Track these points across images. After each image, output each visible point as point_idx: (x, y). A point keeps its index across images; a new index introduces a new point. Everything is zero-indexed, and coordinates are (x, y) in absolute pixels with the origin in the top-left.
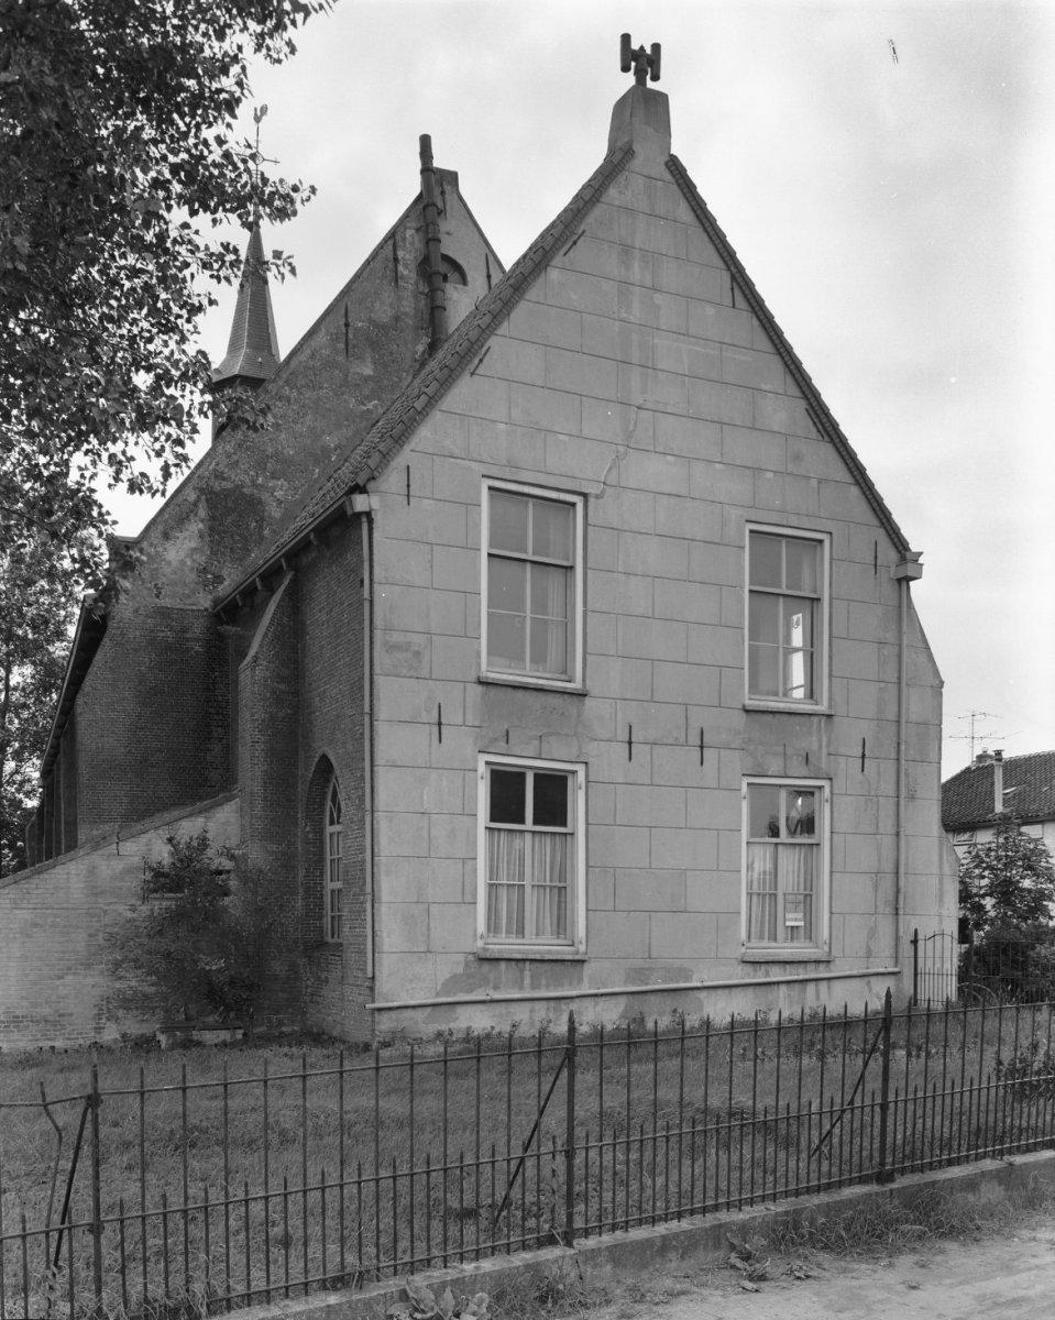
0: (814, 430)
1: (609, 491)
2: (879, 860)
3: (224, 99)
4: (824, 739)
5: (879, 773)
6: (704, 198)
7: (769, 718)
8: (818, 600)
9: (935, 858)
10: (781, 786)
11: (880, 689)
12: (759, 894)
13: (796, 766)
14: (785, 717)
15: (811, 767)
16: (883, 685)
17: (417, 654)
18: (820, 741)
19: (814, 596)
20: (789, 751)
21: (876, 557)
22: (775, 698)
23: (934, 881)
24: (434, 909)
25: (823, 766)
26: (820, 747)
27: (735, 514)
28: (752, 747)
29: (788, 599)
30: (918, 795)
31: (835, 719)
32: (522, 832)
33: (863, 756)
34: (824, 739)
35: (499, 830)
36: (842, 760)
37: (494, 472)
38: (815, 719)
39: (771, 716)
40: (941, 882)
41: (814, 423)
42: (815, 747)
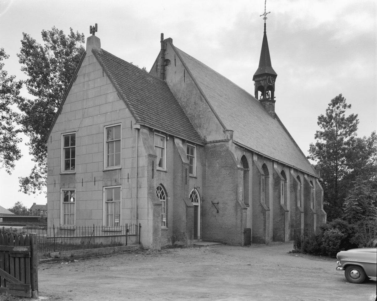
0: (119, 98)
1: (80, 129)
2: (132, 205)
3: (352, 169)
4: (119, 175)
5: (132, 182)
6: (287, 129)
7: (108, 172)
8: (163, 148)
9: (147, 202)
10: (113, 188)
11: (132, 159)
12: (111, 215)
13: (114, 183)
14: (111, 171)
15: (117, 183)
16: (133, 158)
17: (52, 171)
18: (118, 176)
19: (163, 147)
20: (112, 180)
21: (131, 125)
22: (113, 167)
23: (147, 210)
24: (54, 219)
25: (119, 182)
26: (119, 177)
27: (102, 126)
28: (104, 180)
29: (117, 142)
30: (141, 187)
31: (122, 170)
32: (68, 203)
33: (128, 178)
34: (119, 175)
35: (66, 203)
36: (123, 180)
37: (63, 132)
38: (117, 170)
39: (108, 172)
40: (148, 210)
41: (119, 96)
42: (117, 177)
